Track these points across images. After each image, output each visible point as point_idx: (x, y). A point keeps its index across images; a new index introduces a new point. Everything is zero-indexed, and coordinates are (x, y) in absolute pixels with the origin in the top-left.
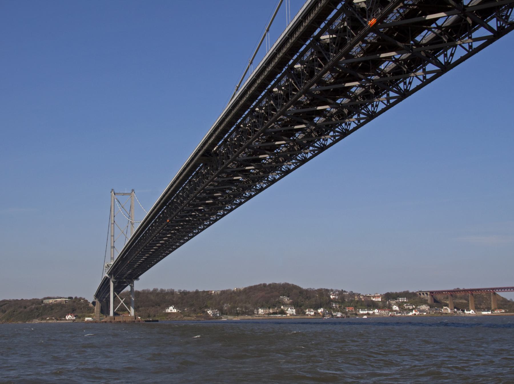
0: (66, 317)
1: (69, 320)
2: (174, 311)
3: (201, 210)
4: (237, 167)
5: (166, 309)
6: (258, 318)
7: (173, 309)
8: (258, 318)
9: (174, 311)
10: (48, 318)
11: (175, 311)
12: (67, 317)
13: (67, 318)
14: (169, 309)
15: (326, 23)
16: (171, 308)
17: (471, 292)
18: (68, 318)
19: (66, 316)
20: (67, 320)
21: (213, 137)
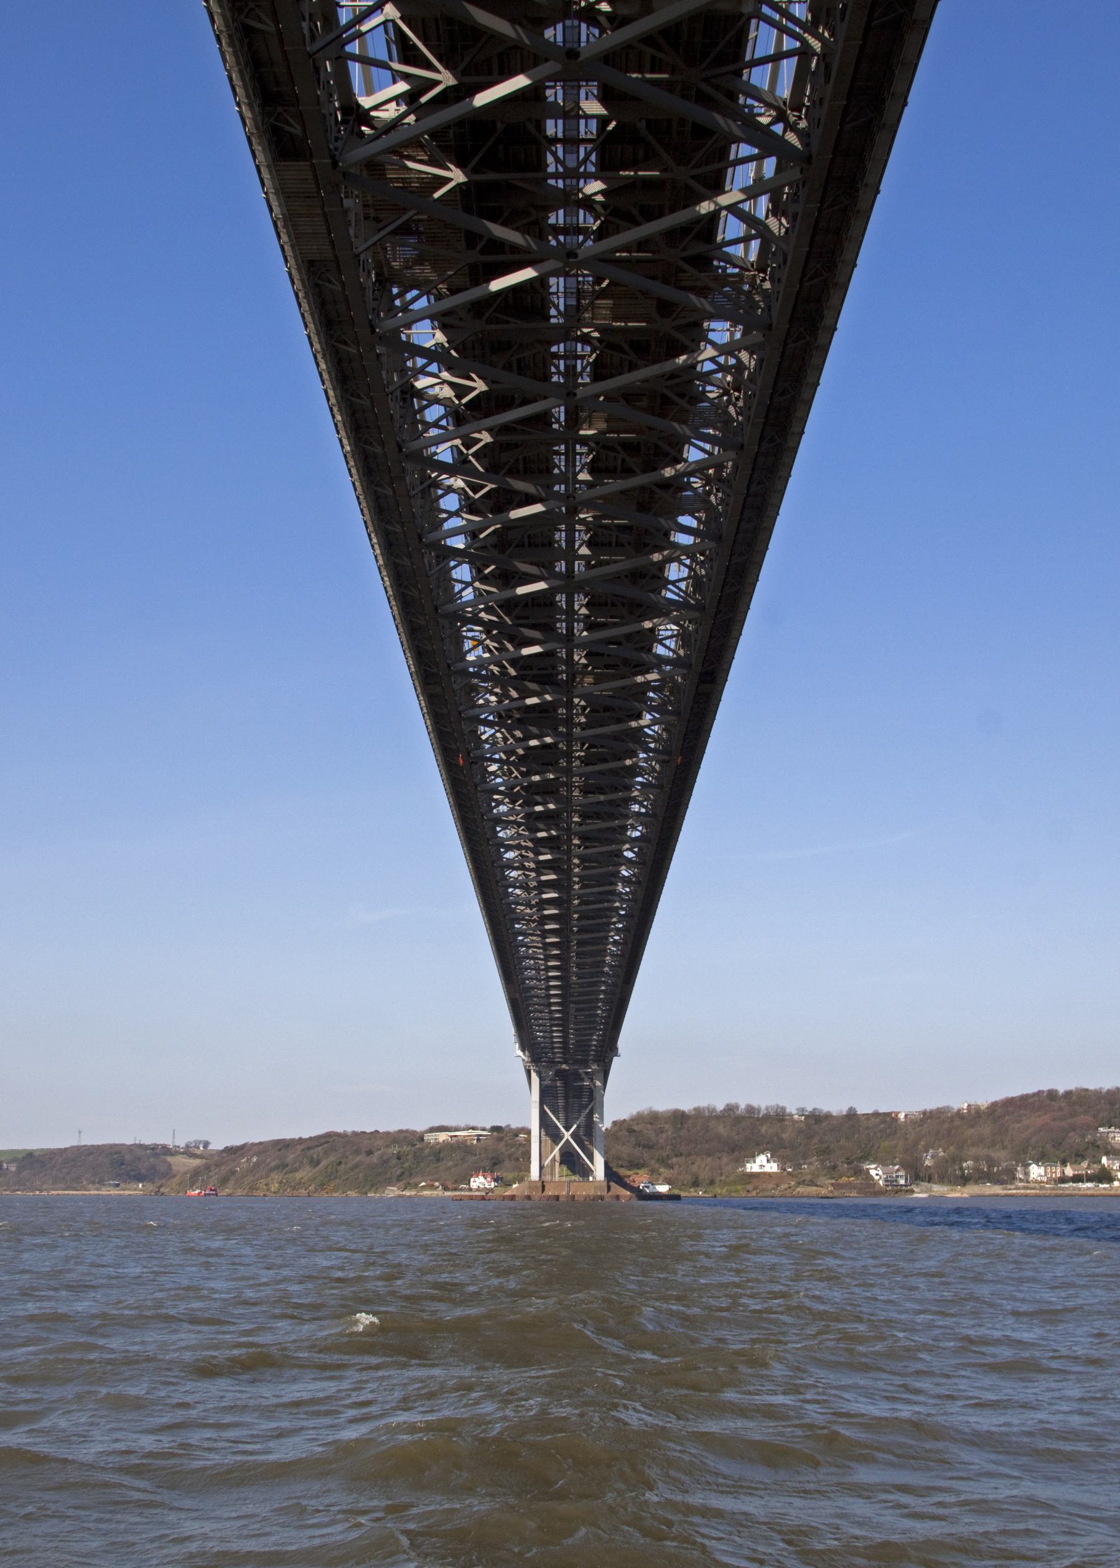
1: (478, 1189)
5: (748, 1162)
7: (768, 1161)
10: (423, 1184)
11: (773, 1167)
12: (475, 1181)
14: (755, 1162)
16: (762, 1159)
20: (471, 1190)
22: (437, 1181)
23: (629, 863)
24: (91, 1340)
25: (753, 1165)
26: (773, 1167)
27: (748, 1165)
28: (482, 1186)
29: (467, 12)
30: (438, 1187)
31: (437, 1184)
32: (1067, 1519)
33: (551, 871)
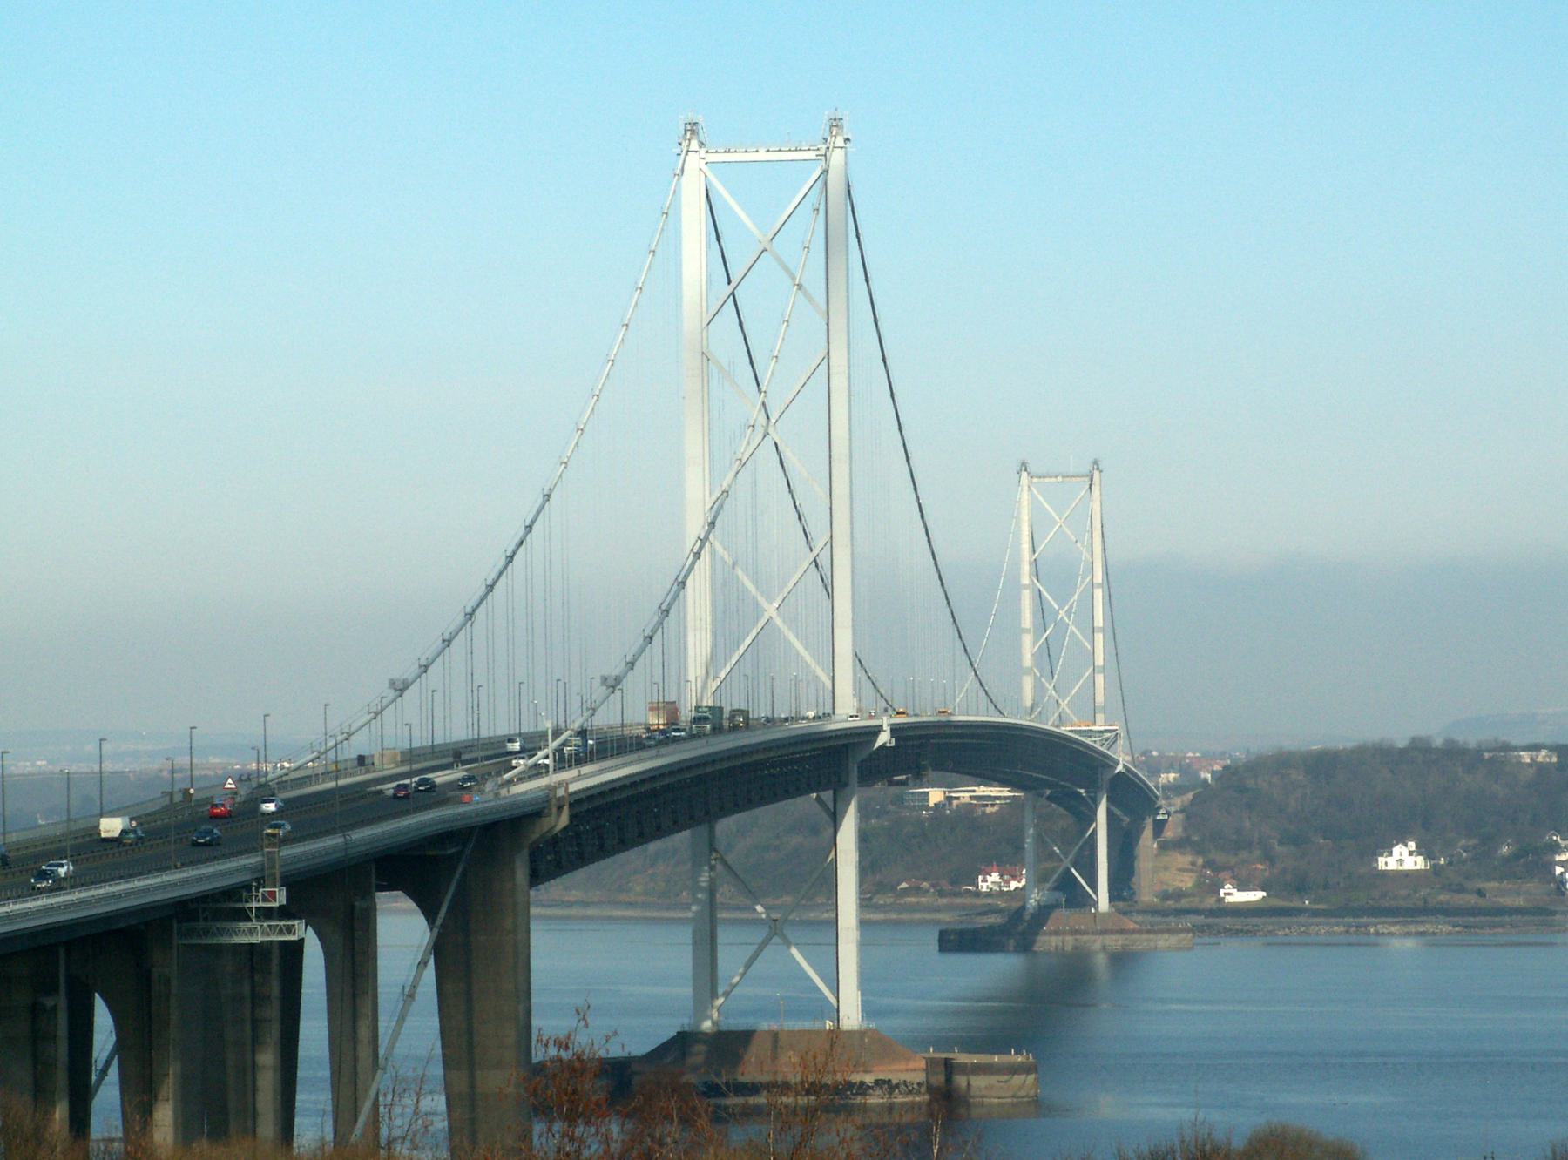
0: (980, 884)
1: (990, 894)
2: (1416, 864)
3: (295, 827)
4: (283, 825)
5: (1382, 855)
6: (985, 1004)
7: (1411, 853)
8: (985, 1004)
9: (1416, 864)
10: (904, 885)
11: (1415, 863)
12: (985, 881)
13: (985, 885)
14: (1391, 854)
15: (830, 792)
16: (1399, 850)
17: (1093, 469)
18: (989, 884)
19: (980, 878)
20: (978, 894)
21: (1138, 782)
22: (925, 879)
23: (742, 722)
24: (1210, 920)
25: (1389, 859)
26: (1415, 863)
27: (1382, 860)
28: (996, 888)
29: (1101, 799)
30: (928, 891)
31: (925, 885)
32: (552, 709)
33: (996, 783)
